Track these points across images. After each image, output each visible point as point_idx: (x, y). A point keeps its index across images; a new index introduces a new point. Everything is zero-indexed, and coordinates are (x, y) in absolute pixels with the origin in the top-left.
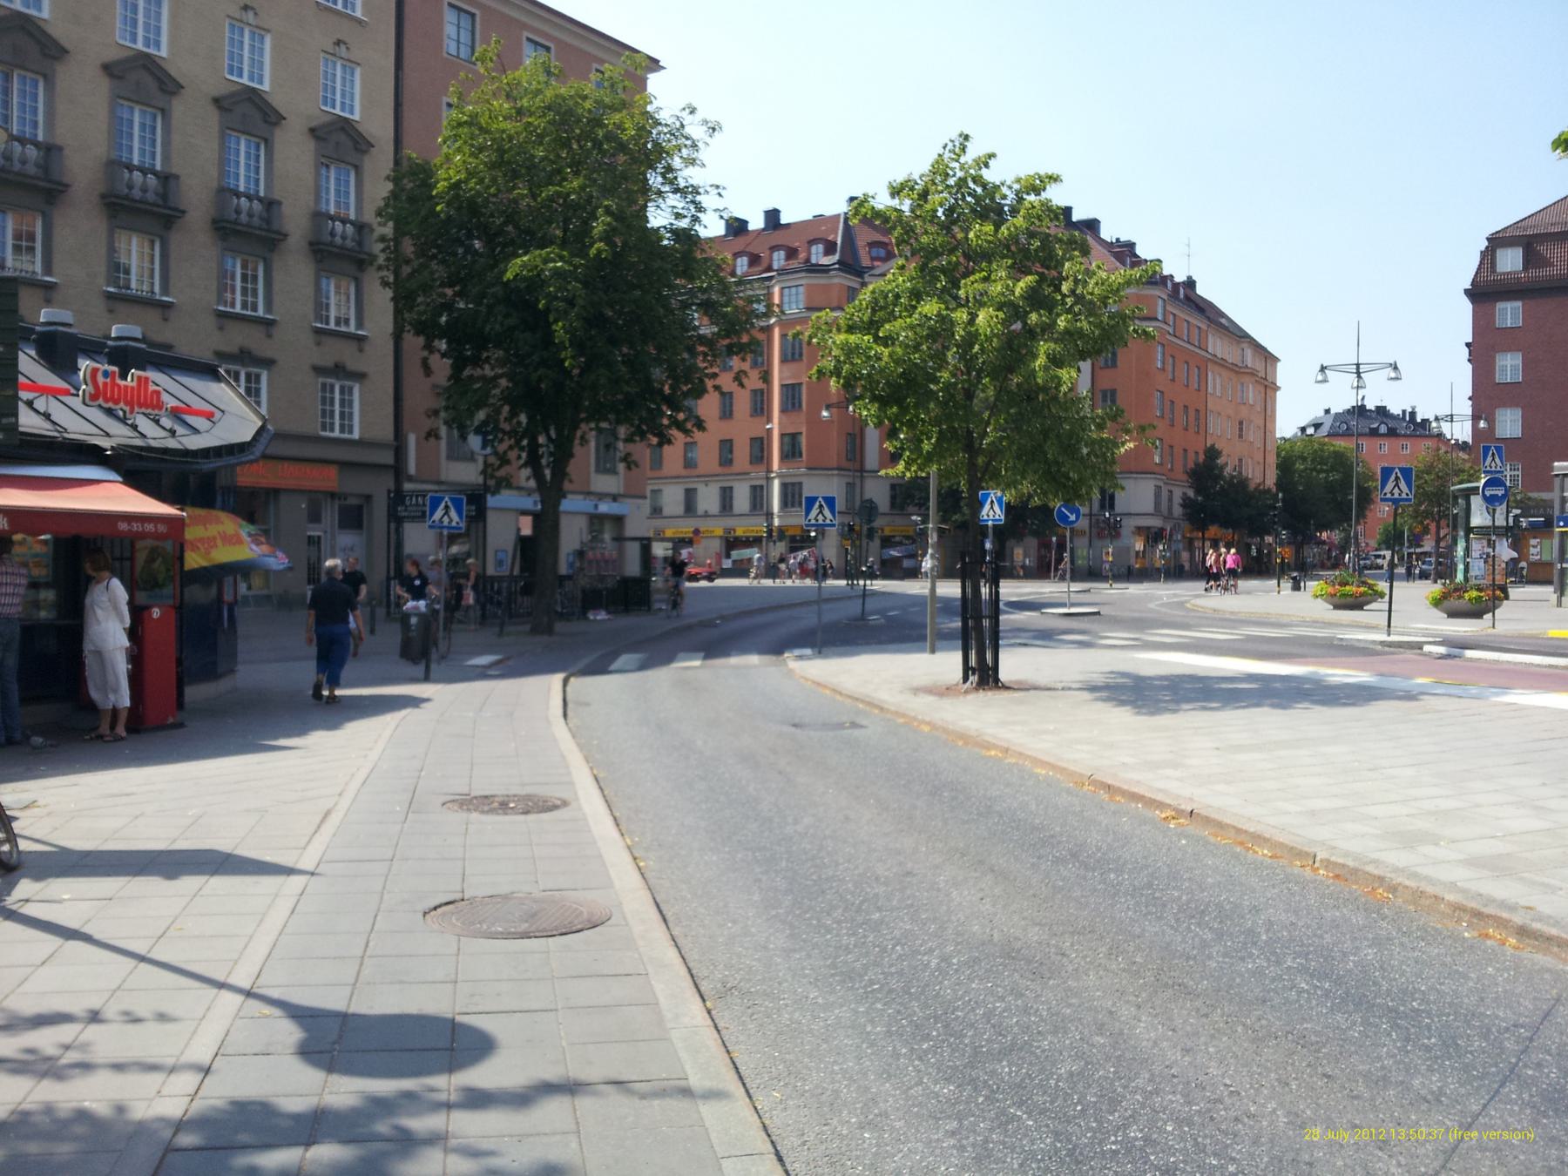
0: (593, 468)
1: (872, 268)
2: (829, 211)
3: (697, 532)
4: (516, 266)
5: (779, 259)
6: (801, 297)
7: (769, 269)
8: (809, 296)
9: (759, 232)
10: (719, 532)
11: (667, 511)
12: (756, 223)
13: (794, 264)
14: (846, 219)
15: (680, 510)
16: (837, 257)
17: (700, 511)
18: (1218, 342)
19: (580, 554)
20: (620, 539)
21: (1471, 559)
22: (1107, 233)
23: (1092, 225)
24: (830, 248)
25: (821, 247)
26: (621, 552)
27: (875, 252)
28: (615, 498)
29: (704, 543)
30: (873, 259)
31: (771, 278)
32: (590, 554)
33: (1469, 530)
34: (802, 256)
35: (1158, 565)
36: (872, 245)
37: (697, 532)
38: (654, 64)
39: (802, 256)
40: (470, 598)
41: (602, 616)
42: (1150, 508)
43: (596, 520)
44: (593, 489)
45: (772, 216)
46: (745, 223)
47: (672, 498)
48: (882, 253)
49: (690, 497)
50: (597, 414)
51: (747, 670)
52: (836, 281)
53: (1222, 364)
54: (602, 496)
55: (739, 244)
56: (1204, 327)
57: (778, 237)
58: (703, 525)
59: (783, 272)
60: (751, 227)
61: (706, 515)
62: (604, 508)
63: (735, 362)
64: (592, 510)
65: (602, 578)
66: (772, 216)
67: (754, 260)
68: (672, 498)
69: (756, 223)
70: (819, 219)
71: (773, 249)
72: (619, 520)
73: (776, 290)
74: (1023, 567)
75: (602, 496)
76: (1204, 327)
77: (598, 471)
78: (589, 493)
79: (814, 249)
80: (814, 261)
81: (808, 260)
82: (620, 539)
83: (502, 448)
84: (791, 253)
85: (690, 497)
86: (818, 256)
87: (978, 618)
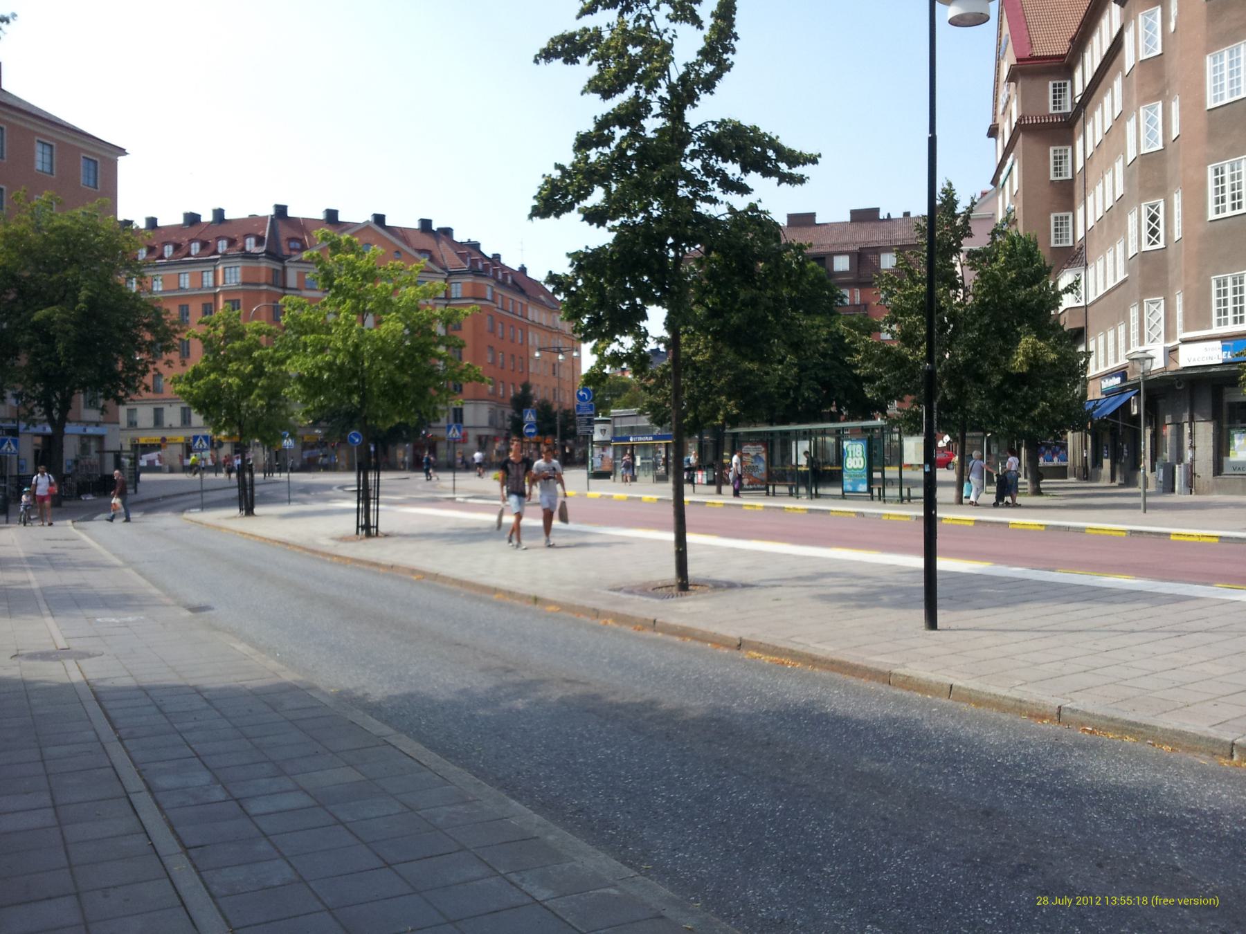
0: (82, 404)
1: (290, 256)
2: (261, 213)
3: (164, 439)
4: (39, 315)
5: (222, 246)
6: (239, 275)
7: (216, 253)
8: (244, 274)
9: (209, 224)
10: (181, 440)
11: (140, 425)
12: (207, 217)
13: (234, 251)
14: (272, 220)
15: (151, 423)
16: (264, 248)
17: (166, 425)
18: (536, 312)
19: (76, 462)
20: (101, 451)
21: (597, 459)
22: (459, 237)
23: (447, 232)
24: (260, 240)
25: (253, 240)
26: (102, 460)
27: (292, 245)
28: (97, 424)
29: (170, 448)
30: (291, 250)
31: (217, 260)
32: (82, 462)
33: (593, 442)
34: (240, 244)
35: (494, 460)
36: (290, 239)
37: (164, 439)
38: (122, 152)
39: (240, 244)
40: (530, 417)
41: (90, 497)
42: (486, 423)
43: (85, 438)
44: (82, 418)
45: (219, 214)
46: (199, 216)
47: (144, 415)
48: (298, 245)
49: (158, 414)
50: (83, 386)
51: (166, 520)
52: (263, 265)
53: (539, 326)
54: (89, 423)
55: (193, 233)
56: (524, 302)
57: (222, 229)
58: (169, 435)
59: (225, 256)
60: (203, 220)
61: (171, 428)
62: (90, 430)
63: (165, 356)
64: (82, 432)
65: (89, 476)
66: (219, 214)
67: (204, 245)
68: (144, 415)
69: (207, 217)
70: (253, 218)
71: (218, 238)
72: (100, 439)
73: (220, 268)
74: (403, 462)
75: (89, 423)
76: (524, 302)
77: (85, 407)
78: (80, 422)
79: (248, 240)
80: (248, 248)
81: (243, 249)
82: (101, 451)
83: (29, 406)
84: (232, 242)
85: (158, 414)
86: (250, 244)
87: (245, 490)
